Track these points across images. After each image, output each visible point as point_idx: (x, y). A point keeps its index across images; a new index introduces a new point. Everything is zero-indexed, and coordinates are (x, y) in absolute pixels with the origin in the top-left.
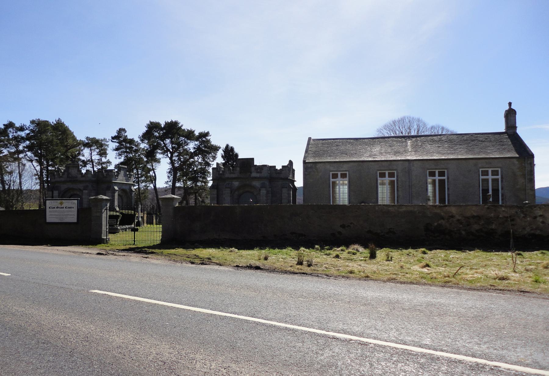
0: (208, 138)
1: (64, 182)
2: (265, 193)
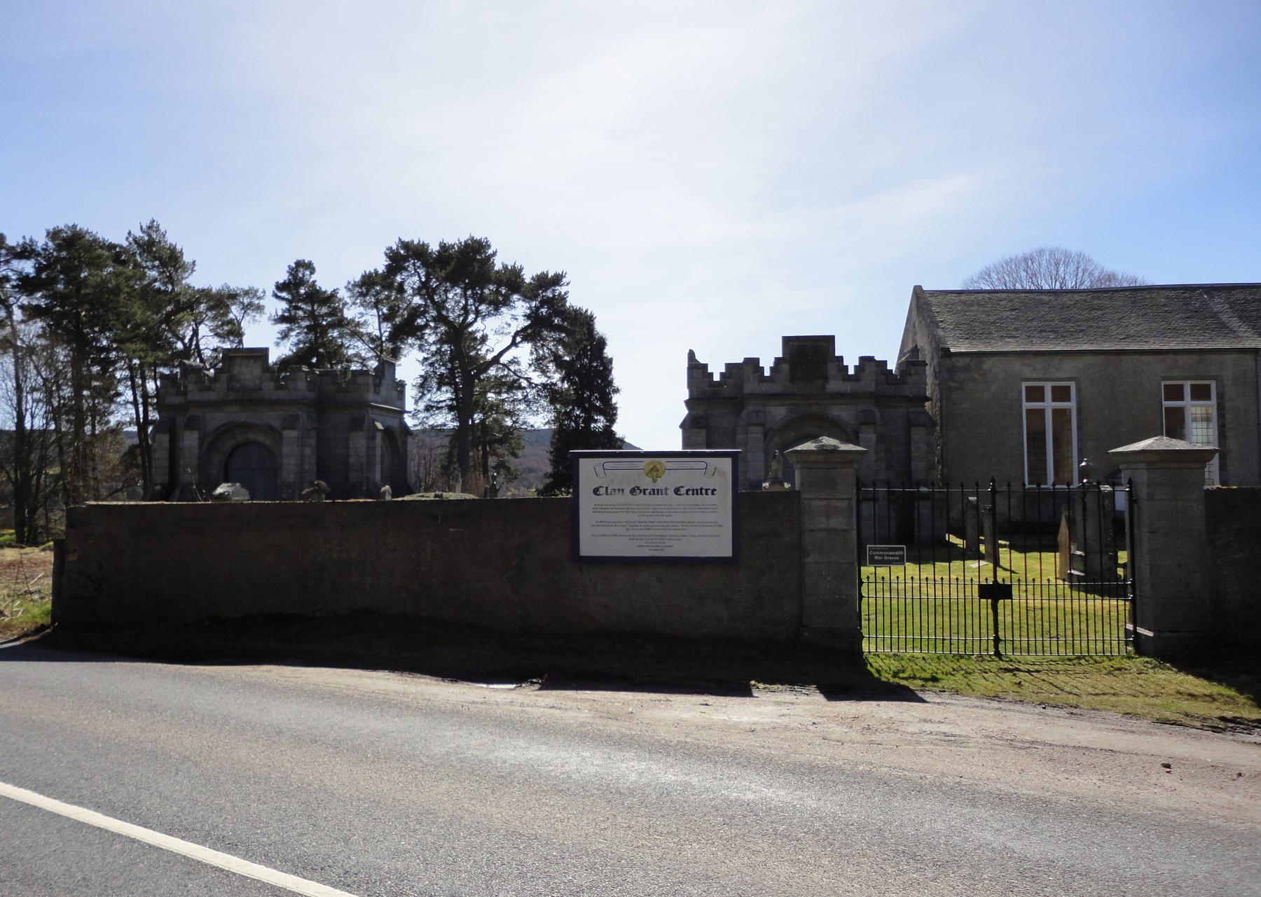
0: (562, 290)
1: (217, 405)
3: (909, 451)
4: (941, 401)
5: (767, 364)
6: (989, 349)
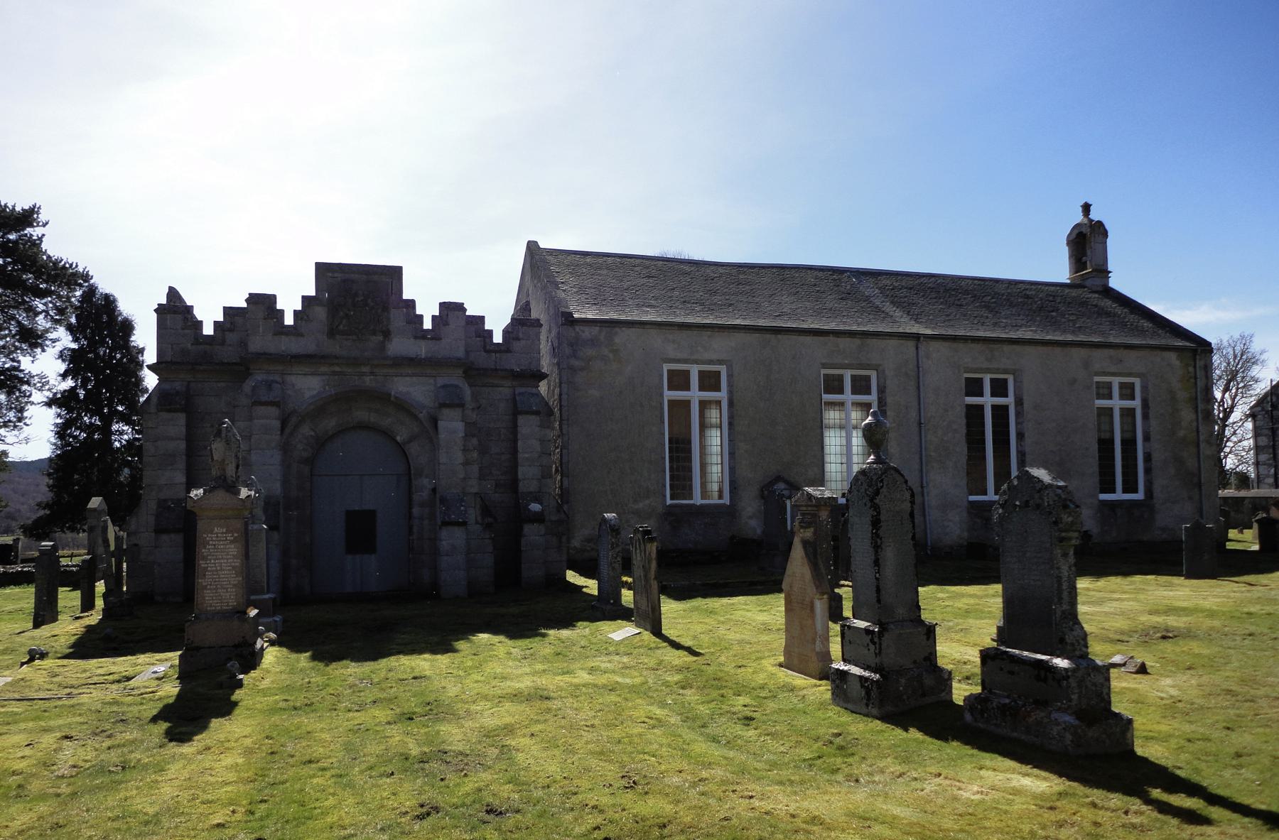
0: (35, 232)
3: (515, 451)
4: (560, 386)
5: (289, 305)
6: (623, 317)
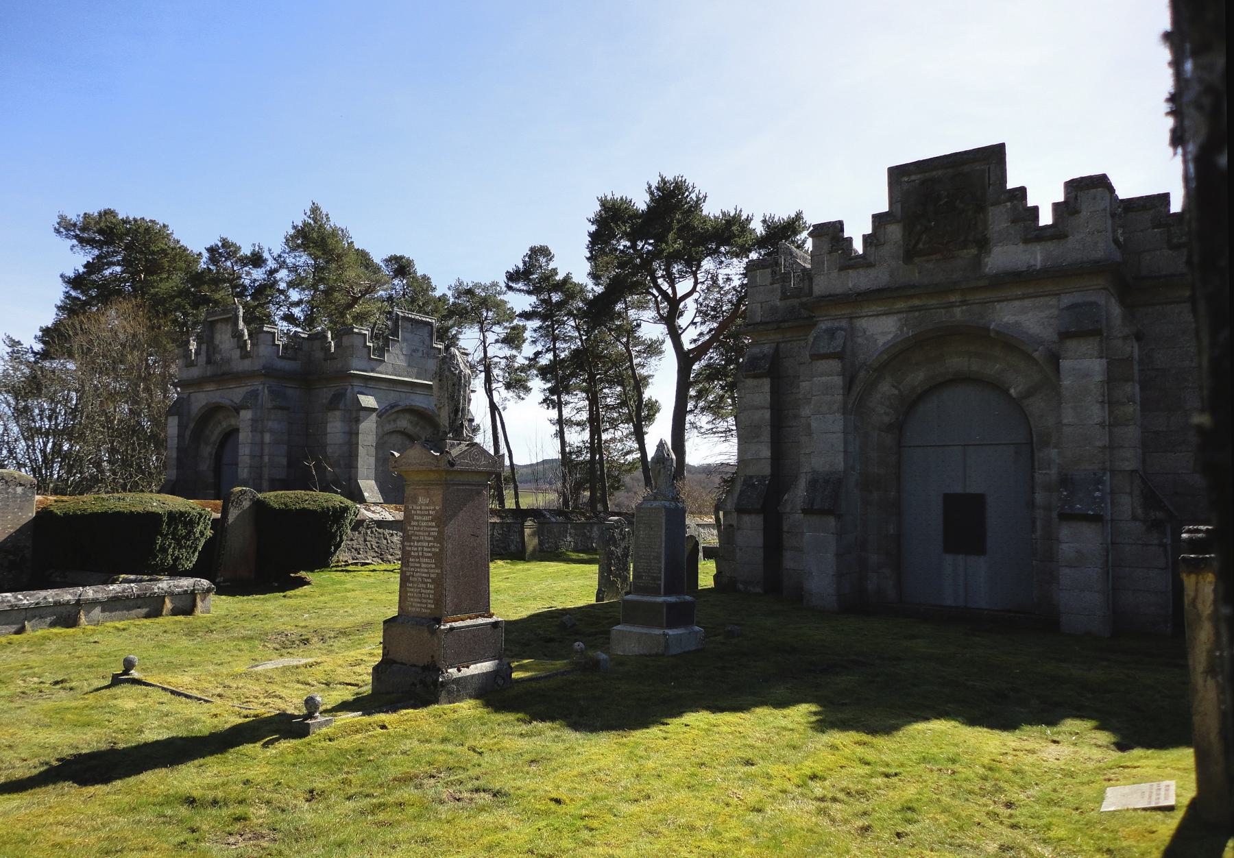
2: (1098, 378)
5: (857, 230)
